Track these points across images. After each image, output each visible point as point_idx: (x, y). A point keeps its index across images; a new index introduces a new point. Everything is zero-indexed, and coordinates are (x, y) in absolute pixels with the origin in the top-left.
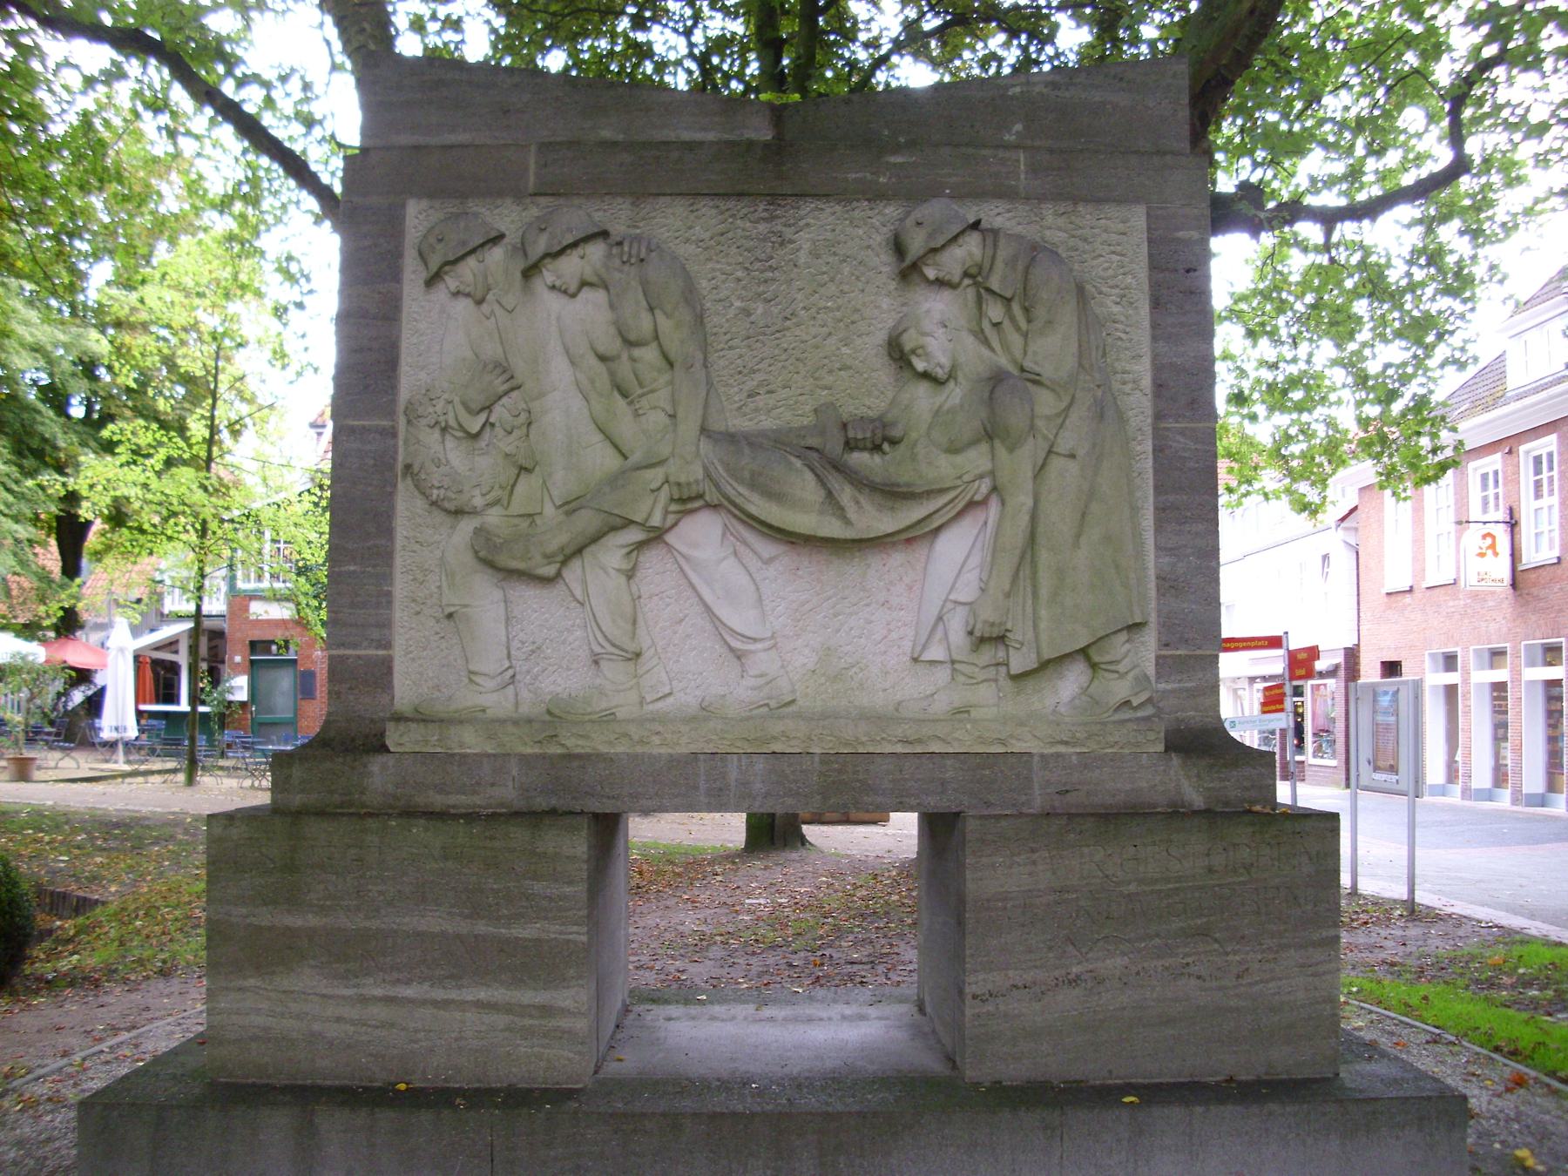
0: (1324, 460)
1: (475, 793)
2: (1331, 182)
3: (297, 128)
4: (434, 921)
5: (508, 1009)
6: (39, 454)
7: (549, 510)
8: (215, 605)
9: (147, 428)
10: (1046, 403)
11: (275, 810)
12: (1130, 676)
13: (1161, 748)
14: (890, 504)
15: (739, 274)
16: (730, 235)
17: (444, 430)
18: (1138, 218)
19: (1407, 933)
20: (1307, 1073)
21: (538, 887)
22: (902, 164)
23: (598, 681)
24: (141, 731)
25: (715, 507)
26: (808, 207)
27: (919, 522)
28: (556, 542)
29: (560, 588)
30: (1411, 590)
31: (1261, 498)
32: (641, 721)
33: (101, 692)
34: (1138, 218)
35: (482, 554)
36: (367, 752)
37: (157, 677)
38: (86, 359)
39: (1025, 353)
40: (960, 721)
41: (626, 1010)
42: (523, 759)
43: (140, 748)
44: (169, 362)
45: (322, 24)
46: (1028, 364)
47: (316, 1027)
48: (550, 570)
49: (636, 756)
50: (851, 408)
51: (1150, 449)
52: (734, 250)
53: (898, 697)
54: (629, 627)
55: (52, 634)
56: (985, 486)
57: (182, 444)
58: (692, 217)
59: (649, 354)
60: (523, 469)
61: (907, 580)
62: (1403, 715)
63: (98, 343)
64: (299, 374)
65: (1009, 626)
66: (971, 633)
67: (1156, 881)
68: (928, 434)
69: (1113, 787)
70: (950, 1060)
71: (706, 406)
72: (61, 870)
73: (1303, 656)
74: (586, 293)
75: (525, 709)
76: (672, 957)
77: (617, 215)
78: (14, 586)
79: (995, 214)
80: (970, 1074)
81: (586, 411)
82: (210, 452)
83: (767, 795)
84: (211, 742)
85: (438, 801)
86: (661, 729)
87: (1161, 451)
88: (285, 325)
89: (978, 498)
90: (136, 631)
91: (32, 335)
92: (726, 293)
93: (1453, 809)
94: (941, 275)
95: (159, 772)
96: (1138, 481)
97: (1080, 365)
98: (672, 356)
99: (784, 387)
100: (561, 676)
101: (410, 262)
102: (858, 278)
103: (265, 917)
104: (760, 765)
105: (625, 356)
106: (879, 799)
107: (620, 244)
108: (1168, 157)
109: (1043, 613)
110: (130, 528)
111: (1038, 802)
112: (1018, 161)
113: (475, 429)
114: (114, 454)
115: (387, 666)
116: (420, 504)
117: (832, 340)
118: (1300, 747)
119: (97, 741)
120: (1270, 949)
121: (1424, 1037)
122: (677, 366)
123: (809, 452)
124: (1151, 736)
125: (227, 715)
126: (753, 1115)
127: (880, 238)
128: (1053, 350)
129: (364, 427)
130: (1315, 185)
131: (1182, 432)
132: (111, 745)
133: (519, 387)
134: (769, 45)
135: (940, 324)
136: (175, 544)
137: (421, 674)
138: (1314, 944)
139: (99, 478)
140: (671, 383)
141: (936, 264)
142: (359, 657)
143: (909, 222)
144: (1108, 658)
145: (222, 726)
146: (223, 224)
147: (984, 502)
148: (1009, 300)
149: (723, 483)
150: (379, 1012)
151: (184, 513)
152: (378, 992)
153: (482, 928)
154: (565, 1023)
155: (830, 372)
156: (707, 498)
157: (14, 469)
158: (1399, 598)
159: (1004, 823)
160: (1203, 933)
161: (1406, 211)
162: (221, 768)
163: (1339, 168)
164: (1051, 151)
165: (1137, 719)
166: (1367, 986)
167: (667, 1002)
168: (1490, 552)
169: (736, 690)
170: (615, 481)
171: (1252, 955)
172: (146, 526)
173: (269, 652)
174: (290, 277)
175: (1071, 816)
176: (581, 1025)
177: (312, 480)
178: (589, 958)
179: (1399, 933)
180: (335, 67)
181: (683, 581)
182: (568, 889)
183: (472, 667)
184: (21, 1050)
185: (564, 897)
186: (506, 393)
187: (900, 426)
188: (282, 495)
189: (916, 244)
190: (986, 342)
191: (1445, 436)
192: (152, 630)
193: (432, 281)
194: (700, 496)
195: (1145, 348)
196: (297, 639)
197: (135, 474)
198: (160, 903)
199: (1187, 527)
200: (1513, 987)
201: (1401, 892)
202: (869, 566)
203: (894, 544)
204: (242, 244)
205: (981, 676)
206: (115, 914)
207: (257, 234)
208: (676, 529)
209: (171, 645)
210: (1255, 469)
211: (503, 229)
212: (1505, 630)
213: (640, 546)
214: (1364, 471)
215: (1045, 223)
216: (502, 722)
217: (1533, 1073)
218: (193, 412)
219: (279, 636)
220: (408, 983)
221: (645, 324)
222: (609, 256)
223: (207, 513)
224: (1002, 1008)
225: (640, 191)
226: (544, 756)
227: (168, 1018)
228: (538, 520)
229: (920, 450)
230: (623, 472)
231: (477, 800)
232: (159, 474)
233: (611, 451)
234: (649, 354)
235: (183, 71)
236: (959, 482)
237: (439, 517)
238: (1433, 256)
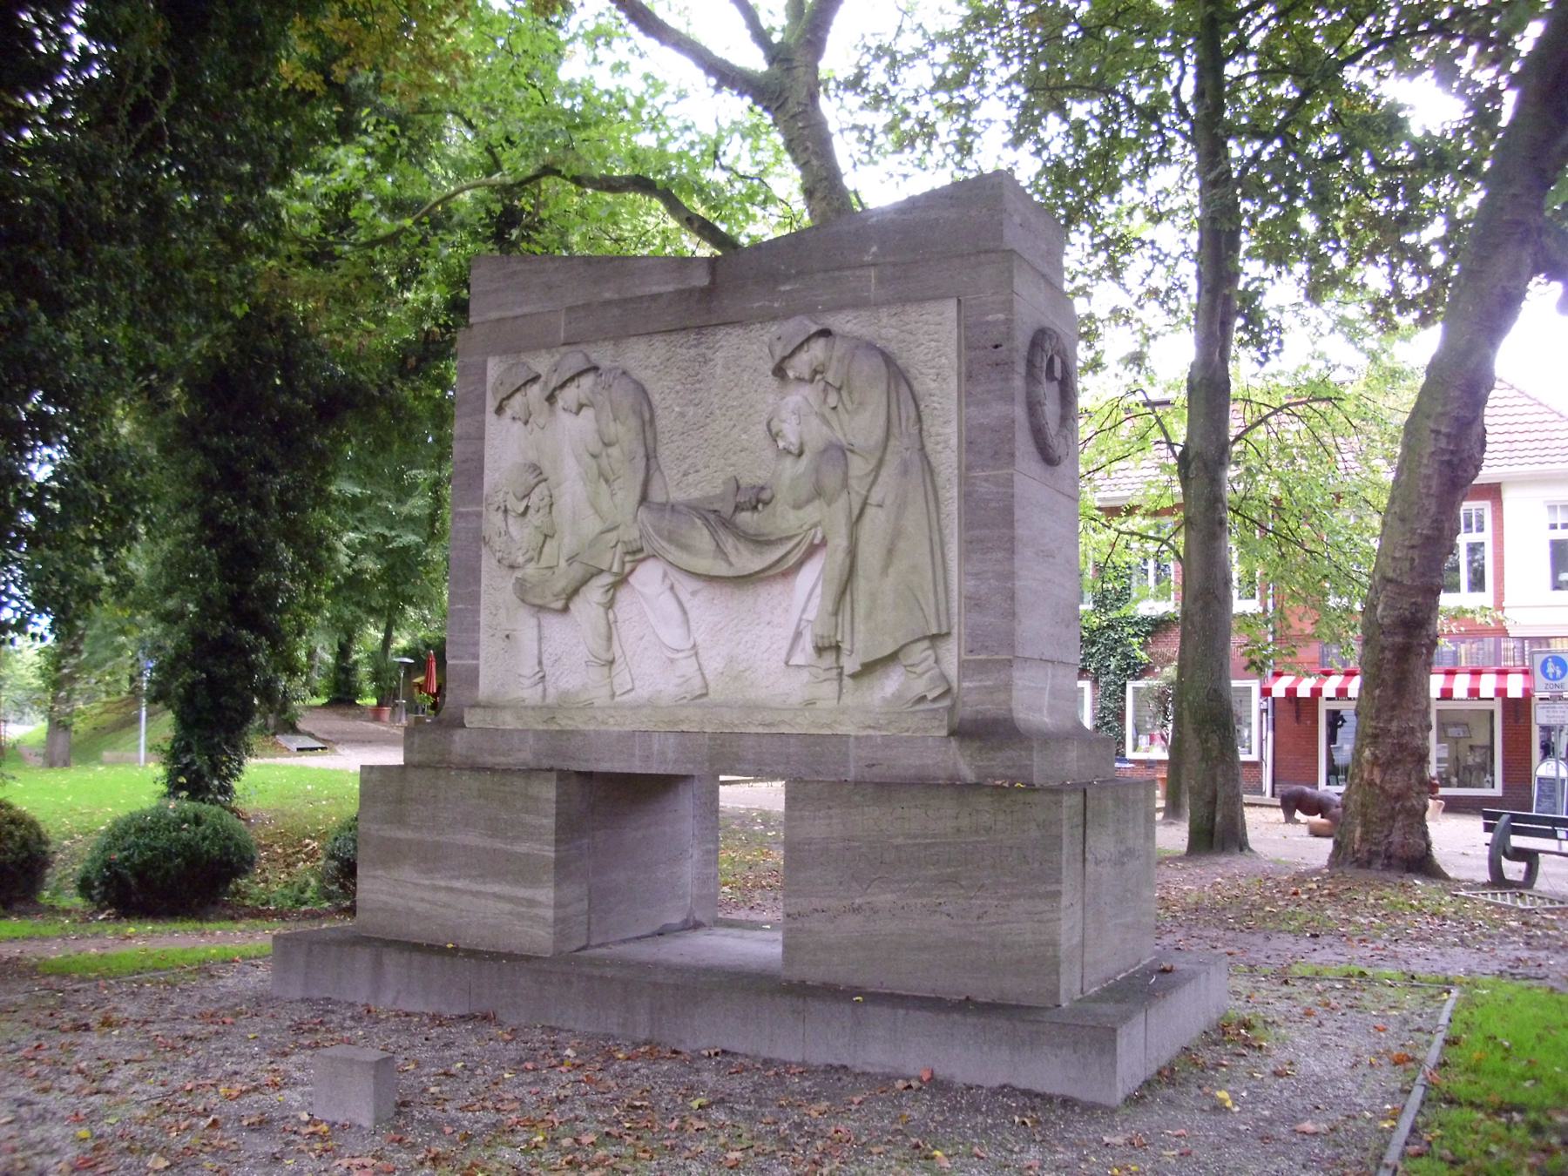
4: (473, 839)
13: (944, 733)
21: (528, 818)
34: (950, 309)
42: (536, 732)
47: (411, 904)
49: (598, 733)
67: (916, 837)
69: (908, 762)
75: (550, 700)
77: (602, 354)
79: (845, 323)
83: (676, 761)
85: (490, 760)
89: (817, 541)
103: (390, 832)
104: (672, 740)
111: (852, 773)
115: (476, 669)
117: (736, 430)
124: (936, 723)
131: (986, 480)
138: (1041, 896)
150: (442, 896)
152: (443, 883)
160: (953, 880)
164: (894, 265)
182: (545, 821)
185: (541, 826)
190: (827, 422)
220: (458, 878)
222: (596, 384)
225: (619, 335)
231: (510, 760)
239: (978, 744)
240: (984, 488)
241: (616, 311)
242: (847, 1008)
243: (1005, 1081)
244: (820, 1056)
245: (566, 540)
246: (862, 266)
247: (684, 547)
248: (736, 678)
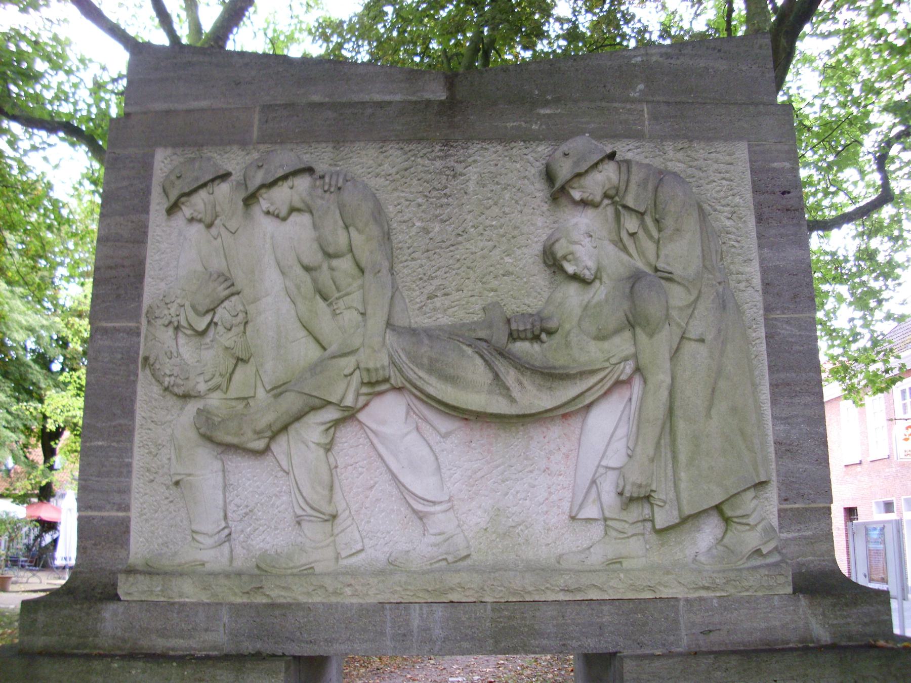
1: (191, 637)
6: (30, 393)
7: (261, 393)
10: (678, 296)
12: (760, 527)
13: (789, 590)
14: (548, 384)
15: (420, 200)
16: (412, 170)
17: (177, 328)
22: (549, 116)
23: (300, 539)
25: (399, 389)
26: (475, 147)
27: (574, 399)
28: (266, 419)
29: (268, 460)
30: (860, 463)
32: (335, 575)
34: (741, 151)
35: (202, 431)
36: (101, 600)
39: (658, 256)
40: (614, 571)
42: (232, 605)
46: (661, 265)
48: (260, 444)
49: (329, 607)
50: (514, 307)
51: (763, 335)
52: (415, 182)
53: (559, 550)
54: (326, 493)
55: (35, 500)
56: (629, 368)
58: (381, 156)
59: (345, 264)
60: (239, 360)
61: (564, 450)
65: (654, 488)
66: (621, 494)
68: (579, 325)
69: (751, 626)
71: (391, 306)
74: (295, 218)
75: (238, 564)
77: (321, 157)
79: (626, 150)
81: (293, 312)
85: (160, 644)
86: (353, 582)
87: (772, 337)
91: (26, 321)
94: (585, 196)
96: (754, 362)
97: (705, 267)
98: (363, 264)
99: (458, 290)
102: (517, 202)
105: (325, 266)
106: (545, 642)
107: (322, 177)
108: (761, 106)
109: (683, 475)
111: (684, 643)
112: (643, 111)
115: (123, 528)
116: (156, 390)
117: (497, 252)
122: (366, 274)
124: (781, 580)
127: (535, 170)
128: (681, 253)
129: (115, 328)
131: (788, 322)
133: (238, 293)
135: (586, 237)
137: (153, 533)
140: (362, 287)
142: (103, 518)
143: (558, 154)
144: (739, 512)
147: (628, 382)
148: (642, 214)
149: (405, 369)
155: (496, 277)
156: (393, 381)
158: (854, 467)
159: (657, 663)
164: (668, 103)
165: (768, 565)
169: (417, 546)
170: (315, 368)
175: (718, 654)
181: (373, 453)
183: (194, 527)
186: (227, 298)
187: (555, 320)
189: (564, 171)
190: (625, 249)
191: (893, 362)
193: (173, 209)
194: (386, 380)
195: (754, 254)
199: (796, 400)
202: (532, 438)
203: (552, 419)
205: (630, 531)
208: (367, 409)
211: (230, 170)
215: (666, 156)
216: (214, 574)
221: (342, 239)
222: (314, 187)
229: (573, 338)
231: (193, 643)
234: (345, 264)
236: (607, 364)
237: (171, 401)
238: (869, 255)
239: (828, 601)
240: (785, 331)
241: (330, 114)
245: (269, 365)
246: (633, 101)
248: (505, 535)
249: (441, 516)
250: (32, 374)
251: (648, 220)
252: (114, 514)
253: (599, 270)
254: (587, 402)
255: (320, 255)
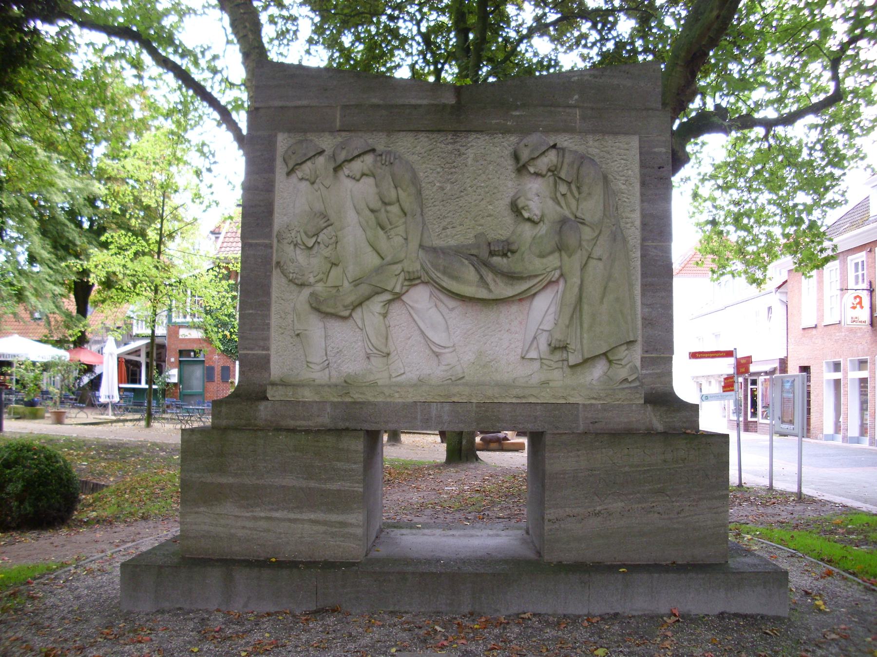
0: (765, 255)
2: (771, 102)
3: (208, 75)
4: (289, 481)
5: (325, 523)
6: (66, 248)
8: (161, 331)
9: (126, 235)
10: (587, 233)
11: (214, 427)
12: (628, 366)
13: (642, 401)
17: (295, 245)
18: (635, 141)
19: (795, 508)
20: (712, 561)
21: (339, 465)
23: (369, 367)
24: (121, 398)
25: (426, 283)
26: (473, 136)
27: (525, 291)
28: (350, 299)
29: (351, 321)
30: (816, 327)
31: (730, 276)
33: (100, 377)
34: (635, 142)
37: (129, 369)
38: (91, 197)
41: (381, 531)
42: (333, 403)
43: (120, 407)
44: (137, 200)
45: (221, 19)
46: (579, 214)
47: (232, 531)
49: (387, 403)
52: (436, 158)
54: (384, 341)
55: (72, 346)
56: (557, 274)
57: (144, 244)
59: (394, 209)
62: (796, 392)
63: (99, 188)
64: (209, 206)
66: (550, 345)
67: (638, 466)
70: (539, 553)
71: (422, 235)
72: (84, 469)
73: (743, 361)
74: (365, 180)
75: (334, 380)
76: (405, 514)
77: (379, 141)
78: (52, 320)
79: (564, 141)
80: (547, 558)
82: (159, 248)
84: (158, 403)
85: (292, 423)
88: (201, 181)
89: (553, 279)
90: (118, 344)
91: (63, 184)
92: (431, 179)
93: (837, 447)
94: (537, 171)
95: (131, 420)
97: (604, 214)
100: (352, 365)
101: (279, 162)
103: (209, 478)
104: (447, 408)
105: (383, 210)
107: (381, 155)
110: (117, 289)
111: (581, 429)
113: (310, 245)
114: (108, 249)
115: (267, 360)
116: (284, 280)
117: (484, 202)
118: (754, 414)
119: (97, 403)
120: (694, 500)
121: (786, 554)
122: (408, 215)
123: (472, 257)
124: (638, 396)
125: (167, 390)
126: (441, 573)
127: (507, 152)
128: (591, 207)
130: (758, 106)
131: (655, 248)
132: (105, 406)
133: (332, 225)
134: (462, 33)
135: (536, 194)
136: (141, 297)
138: (716, 498)
139: (99, 262)
140: (405, 223)
141: (535, 165)
143: (522, 144)
144: (617, 358)
145: (164, 396)
146: (169, 125)
147: (556, 282)
149: (431, 273)
150: (263, 524)
151: (145, 281)
152: (262, 514)
153: (312, 484)
154: (352, 530)
157: (53, 256)
158: (810, 331)
159: (564, 437)
160: (661, 492)
161: (811, 119)
162: (164, 419)
163: (774, 95)
164: (592, 109)
166: (765, 531)
167: (401, 528)
168: (858, 306)
169: (436, 372)
171: (685, 503)
172: (125, 288)
173: (189, 356)
174: (203, 154)
175: (597, 434)
176: (359, 531)
177: (214, 263)
178: (366, 500)
179: (791, 508)
180: (228, 42)
181: (410, 319)
182: (354, 466)
184: (81, 550)
185: (352, 470)
186: (326, 227)
188: (198, 271)
189: (525, 155)
190: (559, 204)
192: (125, 344)
193: (289, 174)
194: (419, 278)
195: (638, 207)
196: (206, 349)
197: (119, 260)
198: (137, 486)
200: (843, 534)
201: (794, 489)
204: (177, 138)
206: (114, 491)
207: (186, 130)
209: (136, 352)
210: (727, 259)
211: (324, 147)
212: (866, 349)
213: (389, 302)
214: (787, 261)
217: (836, 570)
218: (150, 226)
219: (196, 347)
220: (277, 510)
221: (393, 194)
222: (375, 161)
223: (158, 281)
224: (562, 526)
225: (390, 129)
226: (343, 403)
227: (152, 537)
228: (341, 289)
230: (382, 266)
231: (310, 423)
232: (131, 260)
233: (375, 254)
234: (394, 209)
235: (146, 43)
237: (293, 287)
238: (826, 145)
242: (620, 577)
243: (723, 610)
244: (599, 608)
246: (570, 106)
247: (452, 277)
248: (485, 366)
249: (449, 355)
250: (68, 232)
251: (573, 187)
252: (260, 352)
253: (542, 216)
254: (533, 292)
255: (380, 203)
